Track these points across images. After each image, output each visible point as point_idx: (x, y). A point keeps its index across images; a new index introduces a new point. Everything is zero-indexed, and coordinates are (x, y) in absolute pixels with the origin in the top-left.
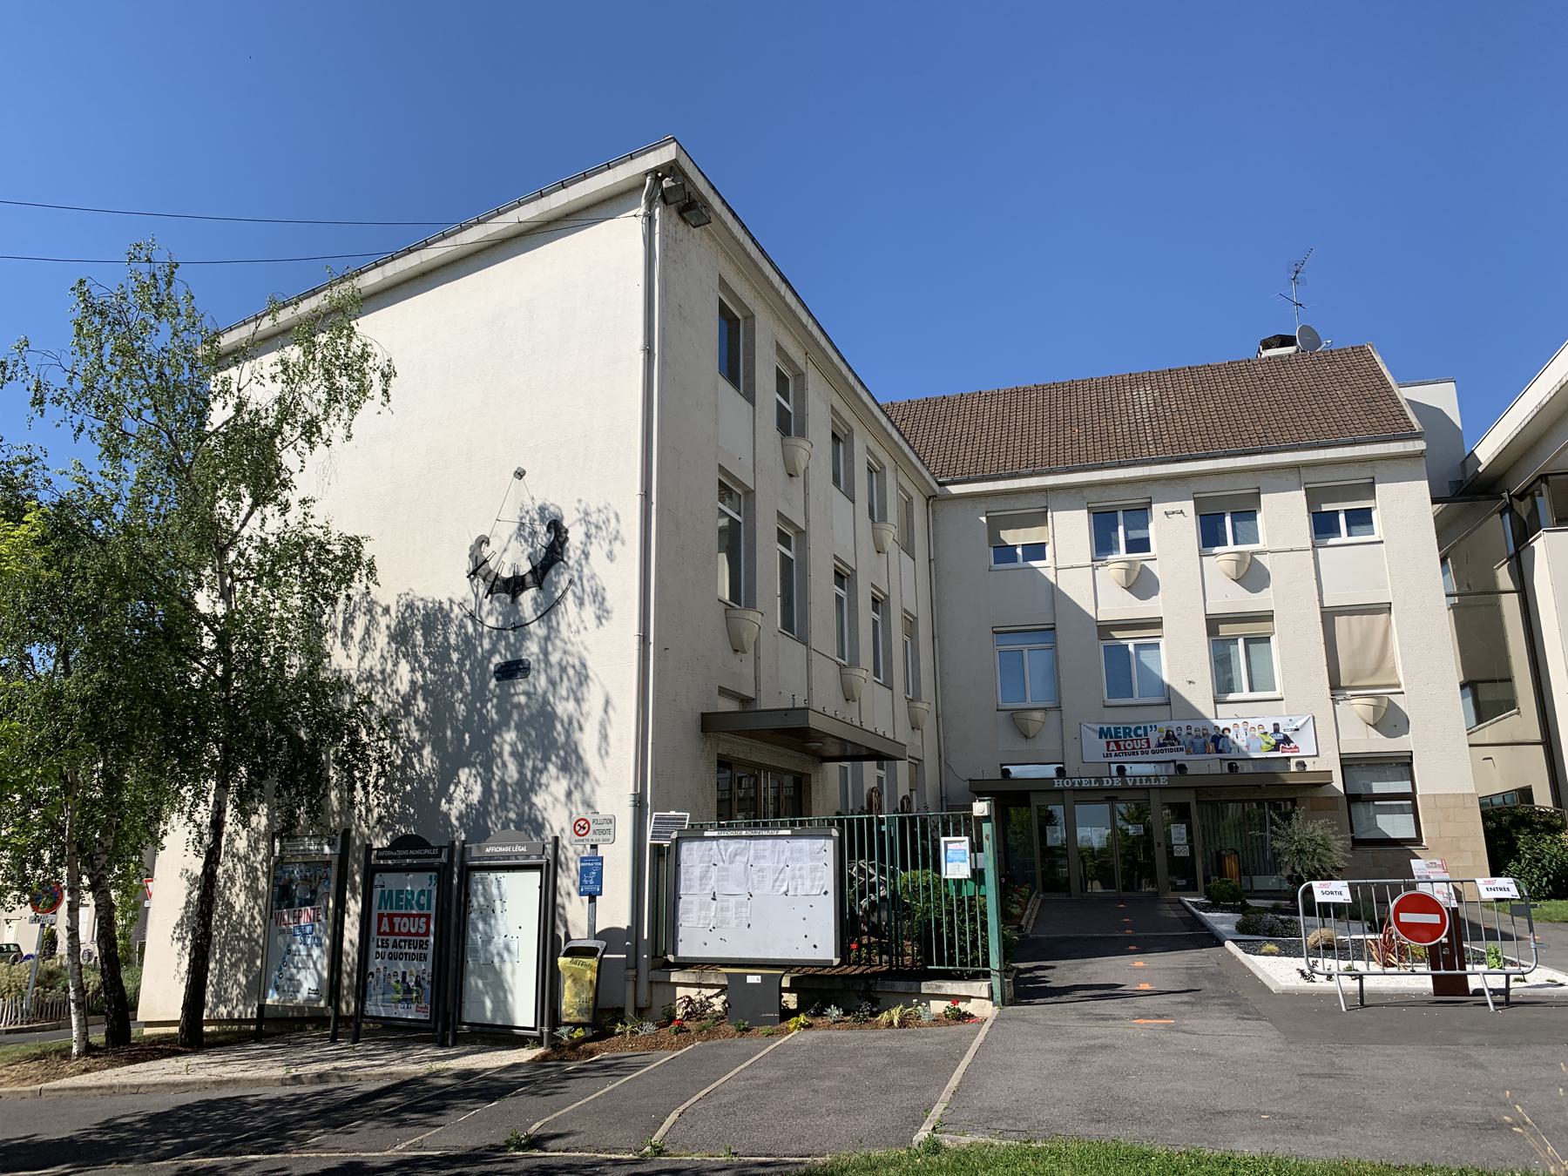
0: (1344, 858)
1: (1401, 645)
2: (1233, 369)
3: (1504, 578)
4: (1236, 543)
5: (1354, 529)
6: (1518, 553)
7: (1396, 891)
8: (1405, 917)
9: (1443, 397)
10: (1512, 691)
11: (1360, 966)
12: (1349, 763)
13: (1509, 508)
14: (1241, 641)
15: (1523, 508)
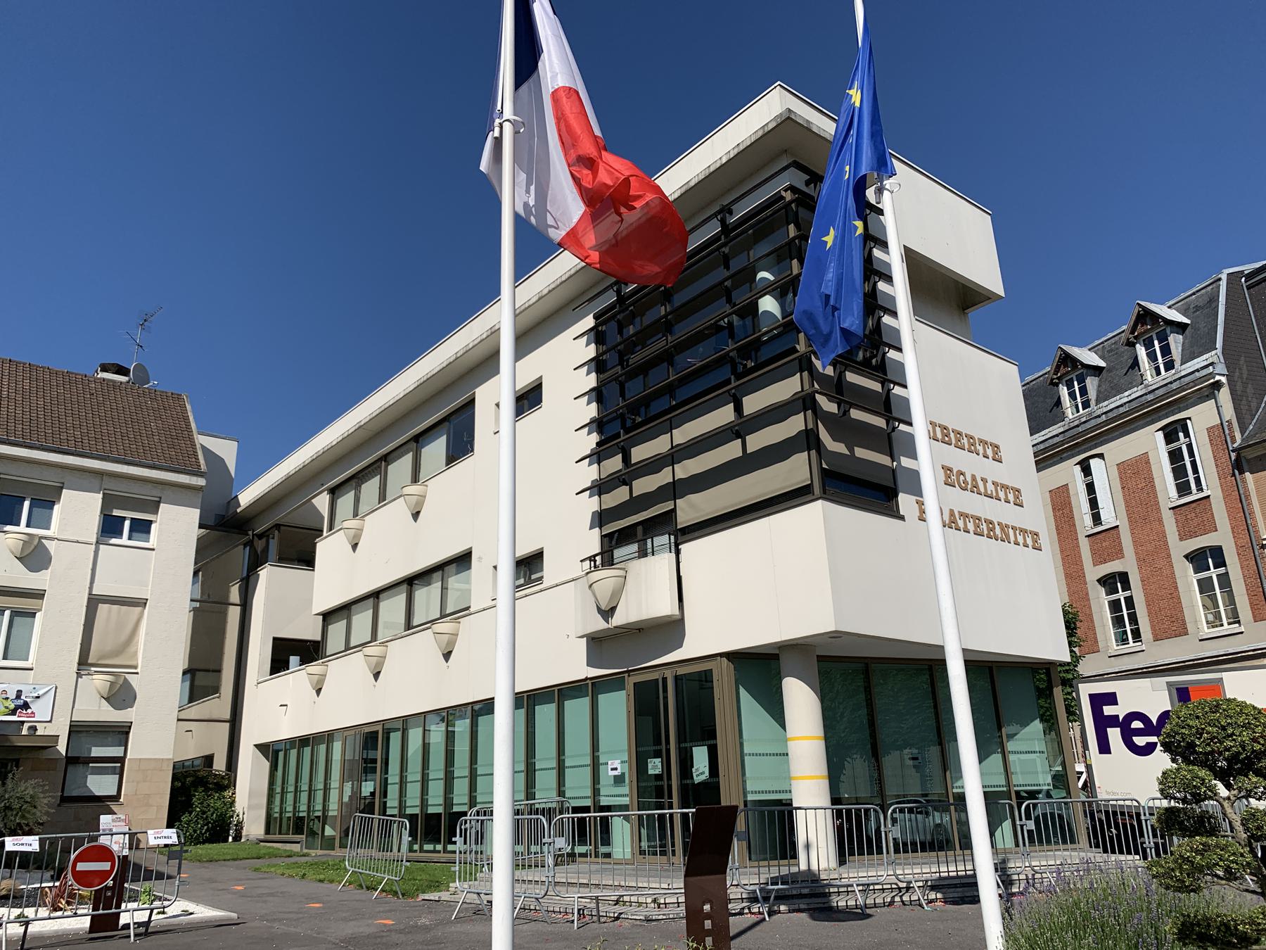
0: (47, 813)
1: (147, 634)
2: (69, 378)
3: (235, 594)
4: (28, 526)
5: (134, 534)
6: (248, 577)
7: (80, 842)
8: (81, 867)
9: (227, 450)
10: (219, 680)
11: (30, 912)
12: (77, 729)
13: (250, 543)
14: (7, 613)
15: (260, 545)
